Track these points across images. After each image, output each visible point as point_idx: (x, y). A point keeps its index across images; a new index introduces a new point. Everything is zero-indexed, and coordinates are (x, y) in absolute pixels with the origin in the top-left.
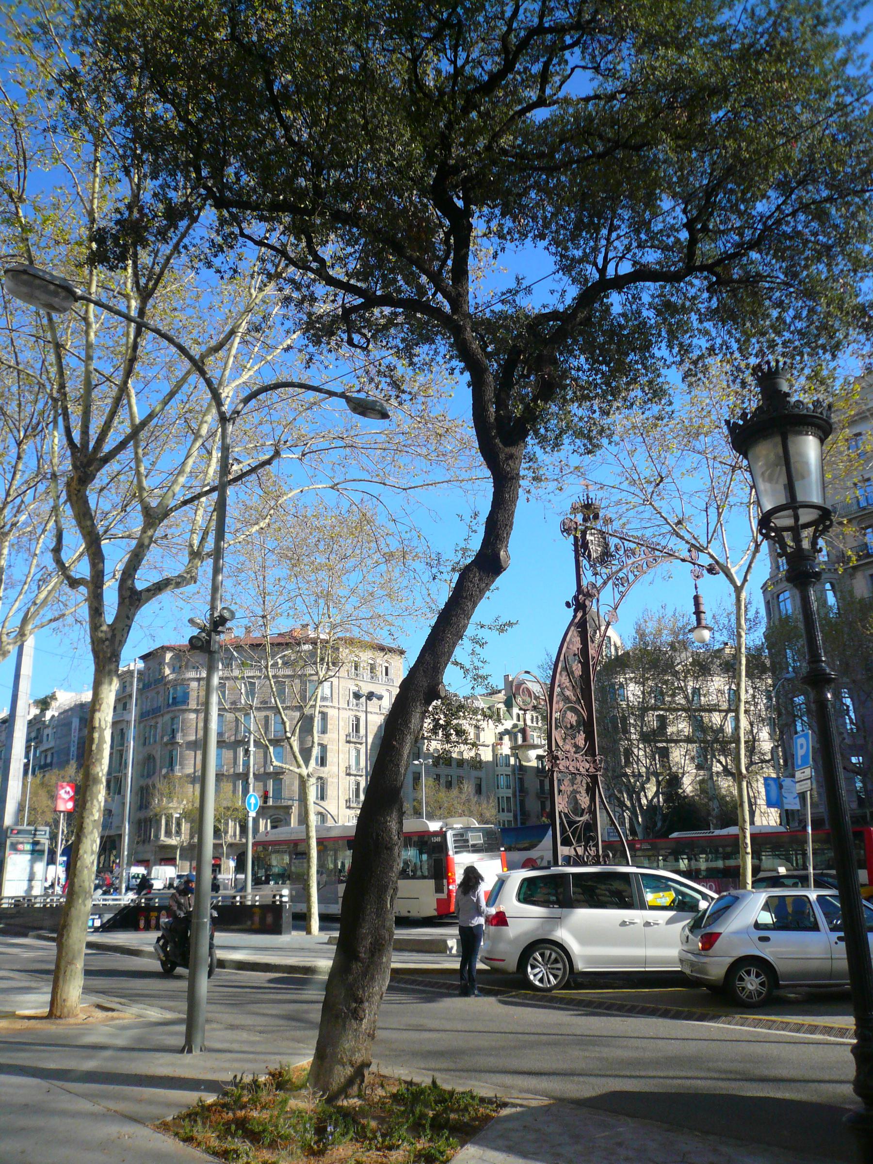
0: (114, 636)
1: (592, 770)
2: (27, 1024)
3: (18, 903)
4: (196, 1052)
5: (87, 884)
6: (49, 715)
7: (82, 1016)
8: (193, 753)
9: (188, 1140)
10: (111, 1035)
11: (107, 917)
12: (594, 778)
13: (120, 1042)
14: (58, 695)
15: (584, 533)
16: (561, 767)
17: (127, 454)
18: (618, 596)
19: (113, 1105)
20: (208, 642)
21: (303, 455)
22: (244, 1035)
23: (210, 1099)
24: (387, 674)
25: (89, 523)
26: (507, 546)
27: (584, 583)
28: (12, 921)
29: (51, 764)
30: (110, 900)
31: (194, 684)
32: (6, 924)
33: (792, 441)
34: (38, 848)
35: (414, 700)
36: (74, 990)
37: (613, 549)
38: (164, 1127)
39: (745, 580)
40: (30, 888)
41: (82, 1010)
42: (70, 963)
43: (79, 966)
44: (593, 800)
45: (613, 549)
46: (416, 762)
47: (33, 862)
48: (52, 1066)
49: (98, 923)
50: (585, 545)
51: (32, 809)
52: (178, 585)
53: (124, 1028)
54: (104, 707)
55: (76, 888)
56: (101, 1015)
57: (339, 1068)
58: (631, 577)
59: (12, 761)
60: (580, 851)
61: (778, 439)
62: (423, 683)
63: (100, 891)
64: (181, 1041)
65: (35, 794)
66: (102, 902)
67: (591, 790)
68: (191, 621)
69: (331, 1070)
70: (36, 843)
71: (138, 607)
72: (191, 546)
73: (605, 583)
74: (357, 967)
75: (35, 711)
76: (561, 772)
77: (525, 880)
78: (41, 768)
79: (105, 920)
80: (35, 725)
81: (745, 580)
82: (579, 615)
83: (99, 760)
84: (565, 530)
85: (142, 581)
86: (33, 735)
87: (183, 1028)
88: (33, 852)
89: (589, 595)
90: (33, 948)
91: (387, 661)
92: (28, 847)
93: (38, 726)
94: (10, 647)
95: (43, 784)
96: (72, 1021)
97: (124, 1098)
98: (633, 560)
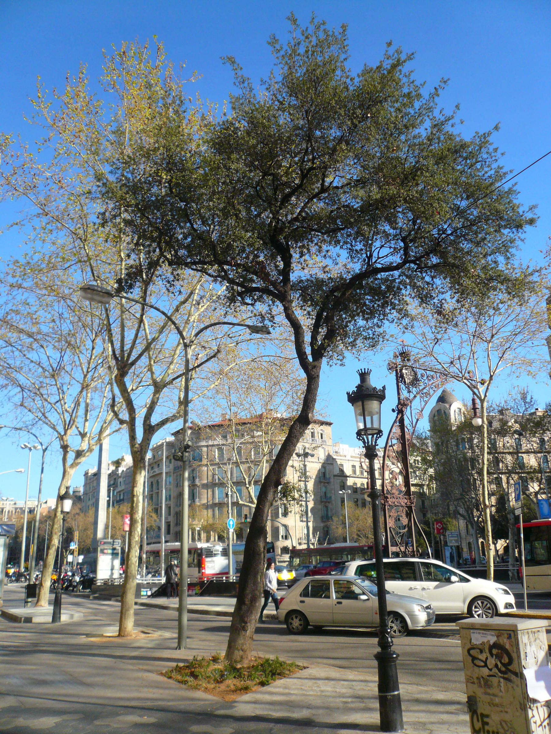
0: (142, 449)
1: (409, 503)
2: (108, 639)
3: (106, 583)
4: (183, 649)
5: (133, 572)
6: (120, 470)
7: (134, 636)
8: (206, 491)
9: (170, 678)
10: (147, 643)
11: (155, 589)
12: (410, 508)
13: (150, 645)
14: (125, 457)
15: (401, 370)
16: (390, 503)
17: (144, 360)
18: (423, 403)
19: (141, 667)
20: (182, 457)
21: (237, 344)
22: (207, 643)
23: (181, 665)
24: (322, 438)
25: (126, 395)
26: (313, 411)
27: (402, 397)
28: (103, 593)
29: (123, 500)
30: (156, 580)
31: (205, 449)
32: (100, 594)
33: (366, 403)
34: (115, 551)
35: (269, 486)
36: (130, 624)
37: (419, 376)
38: (162, 674)
39: (485, 396)
40: (112, 574)
41: (134, 633)
42: (128, 610)
43: (132, 612)
44: (410, 520)
45: (419, 376)
46: (341, 492)
47: (113, 559)
48: (118, 654)
49: (149, 593)
50: (402, 376)
51: (113, 527)
52: (173, 420)
53: (153, 640)
54: (138, 485)
55: (129, 574)
56: (143, 635)
57: (236, 652)
58: (431, 392)
59: (100, 500)
60: (403, 549)
61: (360, 403)
62: (274, 478)
63: (150, 575)
64: (176, 645)
65: (114, 518)
66: (151, 582)
67: (408, 515)
68: (449, 79)
69: (233, 653)
70: (114, 549)
71: (153, 434)
72: (180, 398)
73: (415, 397)
74: (244, 608)
75: (112, 468)
76: (390, 506)
77: (358, 566)
78: (117, 502)
79: (153, 592)
80: (113, 476)
81: (485, 396)
82: (399, 416)
83: (137, 512)
84: (390, 369)
85: (155, 420)
86: (112, 482)
87: (177, 640)
88: (113, 554)
89: (405, 405)
90: (113, 605)
91: (322, 430)
92: (110, 551)
93: (115, 477)
94: (94, 447)
95: (119, 512)
96: (129, 638)
97: (147, 665)
98: (432, 381)
